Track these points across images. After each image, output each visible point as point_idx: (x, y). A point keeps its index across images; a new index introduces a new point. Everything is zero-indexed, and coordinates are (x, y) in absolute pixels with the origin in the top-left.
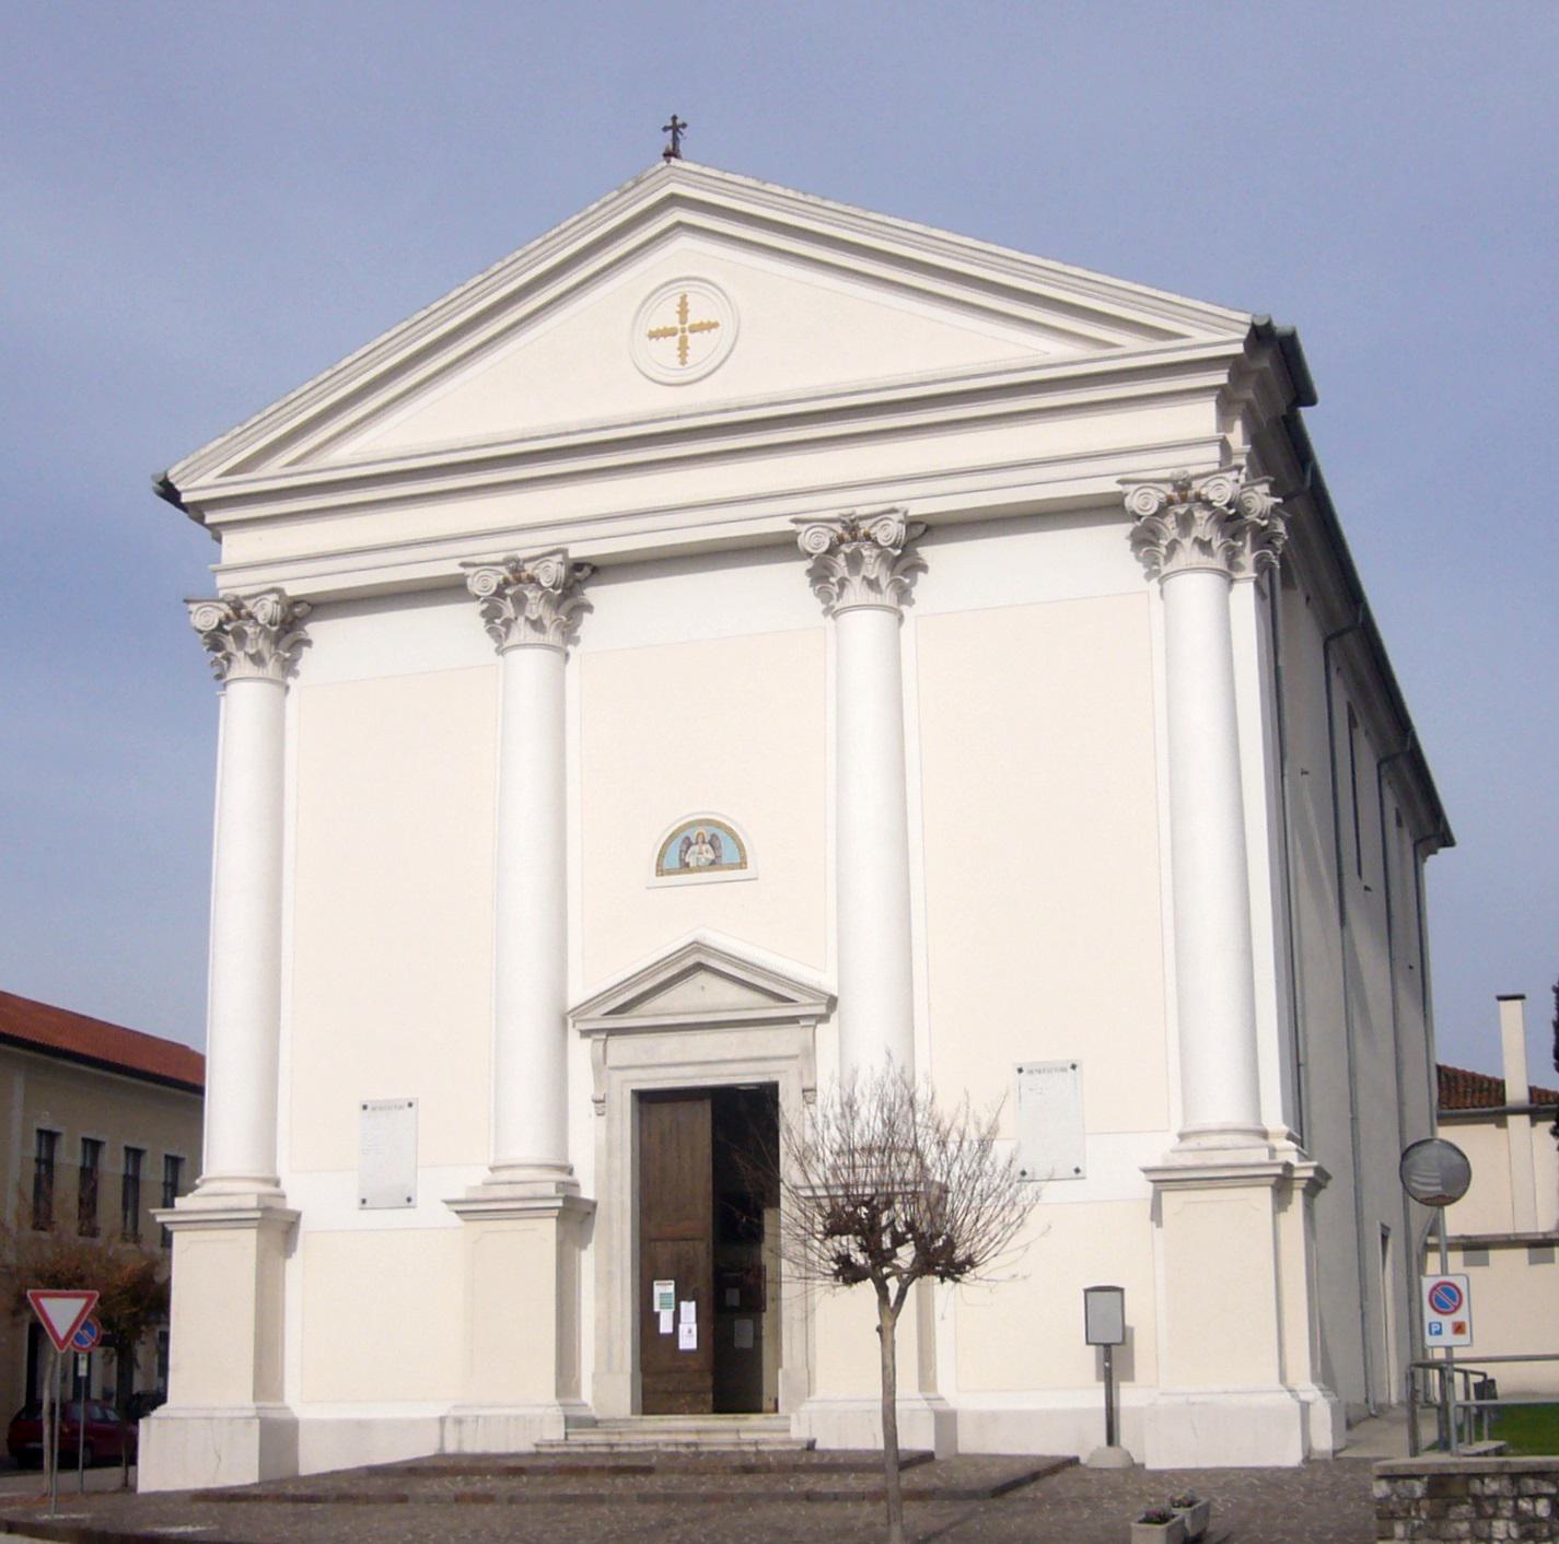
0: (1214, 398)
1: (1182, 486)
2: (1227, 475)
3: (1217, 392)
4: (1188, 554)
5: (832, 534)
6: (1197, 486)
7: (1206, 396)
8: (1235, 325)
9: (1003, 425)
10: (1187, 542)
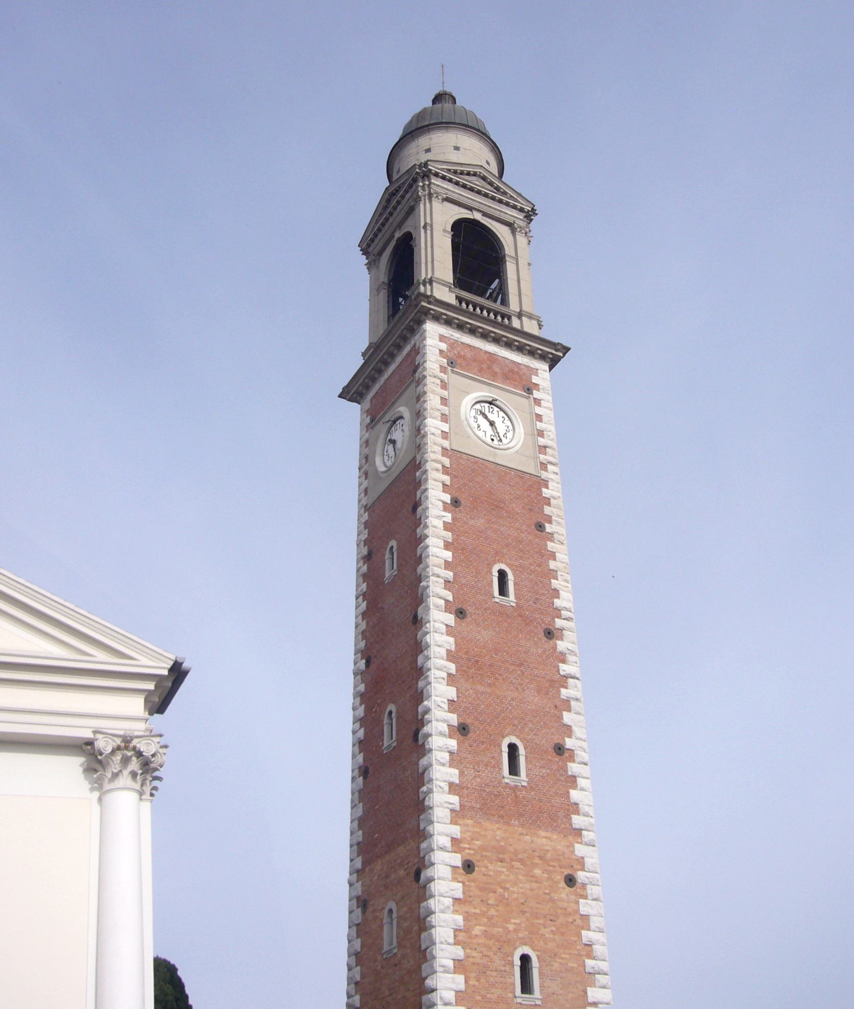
0: (144, 696)
1: (127, 740)
2: (154, 739)
3: (147, 693)
4: (125, 780)
5: (114, 744)
6: (135, 742)
7: (137, 694)
8: (165, 659)
9: (115, 694)
10: (126, 773)
